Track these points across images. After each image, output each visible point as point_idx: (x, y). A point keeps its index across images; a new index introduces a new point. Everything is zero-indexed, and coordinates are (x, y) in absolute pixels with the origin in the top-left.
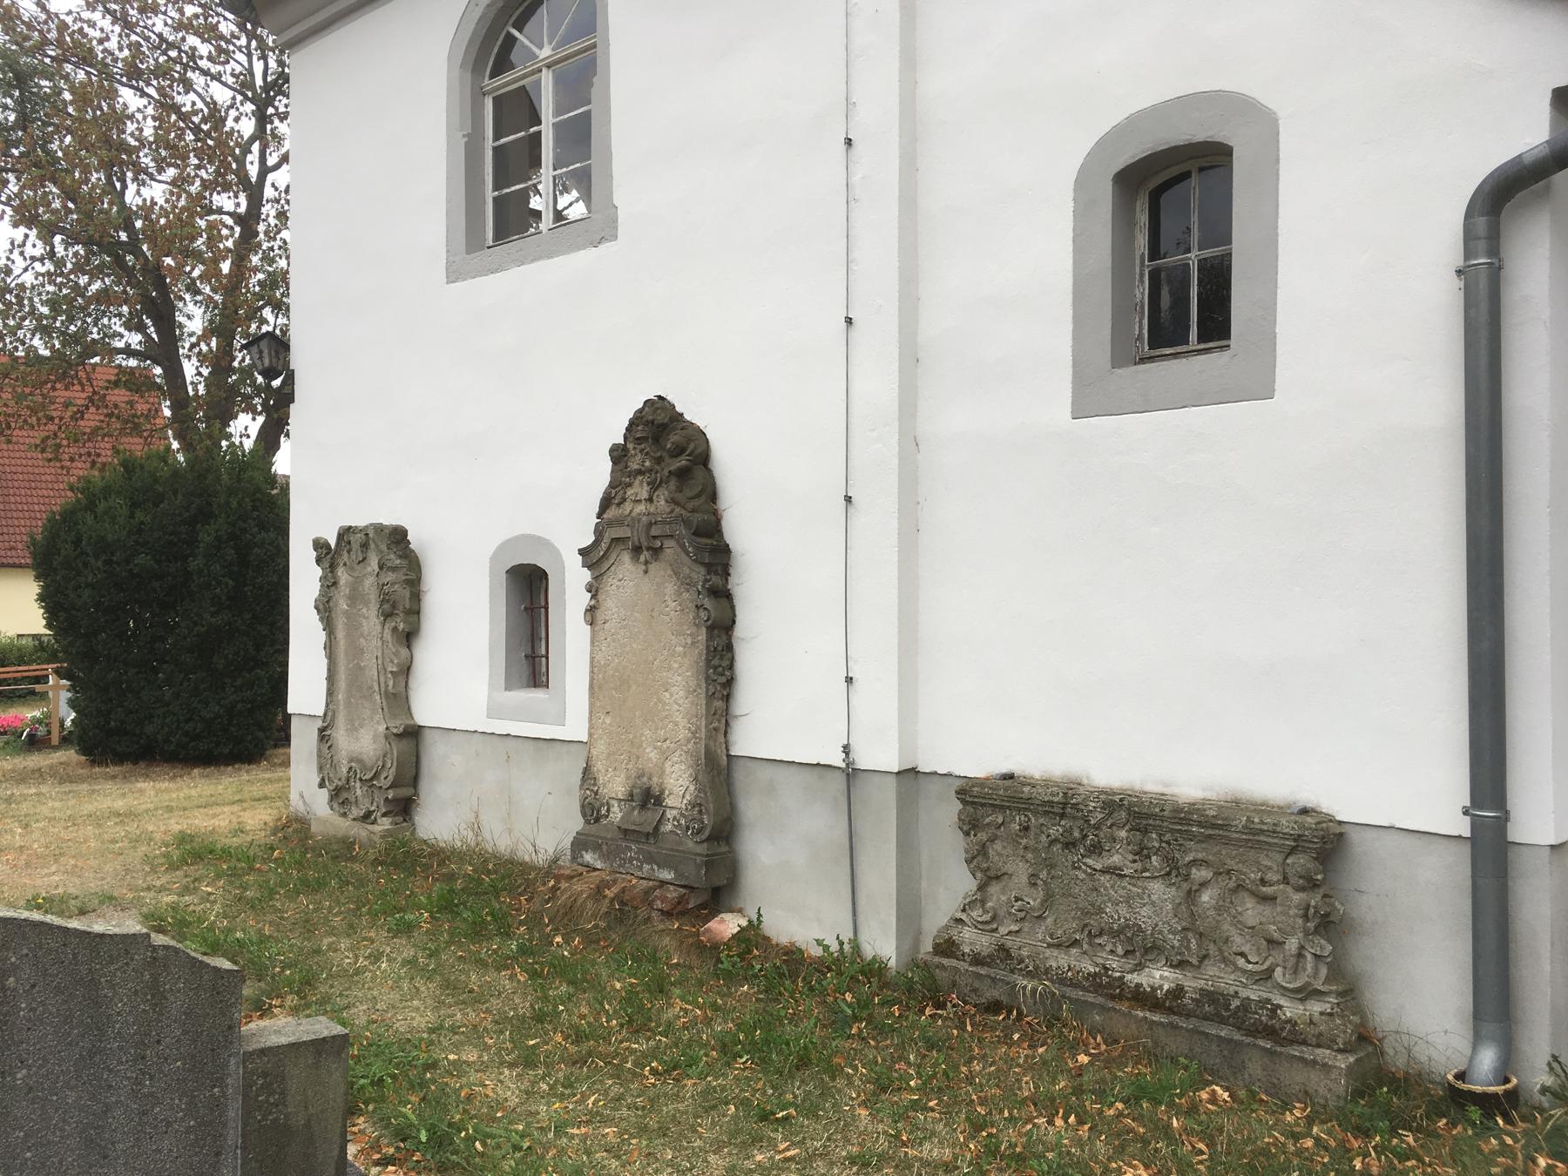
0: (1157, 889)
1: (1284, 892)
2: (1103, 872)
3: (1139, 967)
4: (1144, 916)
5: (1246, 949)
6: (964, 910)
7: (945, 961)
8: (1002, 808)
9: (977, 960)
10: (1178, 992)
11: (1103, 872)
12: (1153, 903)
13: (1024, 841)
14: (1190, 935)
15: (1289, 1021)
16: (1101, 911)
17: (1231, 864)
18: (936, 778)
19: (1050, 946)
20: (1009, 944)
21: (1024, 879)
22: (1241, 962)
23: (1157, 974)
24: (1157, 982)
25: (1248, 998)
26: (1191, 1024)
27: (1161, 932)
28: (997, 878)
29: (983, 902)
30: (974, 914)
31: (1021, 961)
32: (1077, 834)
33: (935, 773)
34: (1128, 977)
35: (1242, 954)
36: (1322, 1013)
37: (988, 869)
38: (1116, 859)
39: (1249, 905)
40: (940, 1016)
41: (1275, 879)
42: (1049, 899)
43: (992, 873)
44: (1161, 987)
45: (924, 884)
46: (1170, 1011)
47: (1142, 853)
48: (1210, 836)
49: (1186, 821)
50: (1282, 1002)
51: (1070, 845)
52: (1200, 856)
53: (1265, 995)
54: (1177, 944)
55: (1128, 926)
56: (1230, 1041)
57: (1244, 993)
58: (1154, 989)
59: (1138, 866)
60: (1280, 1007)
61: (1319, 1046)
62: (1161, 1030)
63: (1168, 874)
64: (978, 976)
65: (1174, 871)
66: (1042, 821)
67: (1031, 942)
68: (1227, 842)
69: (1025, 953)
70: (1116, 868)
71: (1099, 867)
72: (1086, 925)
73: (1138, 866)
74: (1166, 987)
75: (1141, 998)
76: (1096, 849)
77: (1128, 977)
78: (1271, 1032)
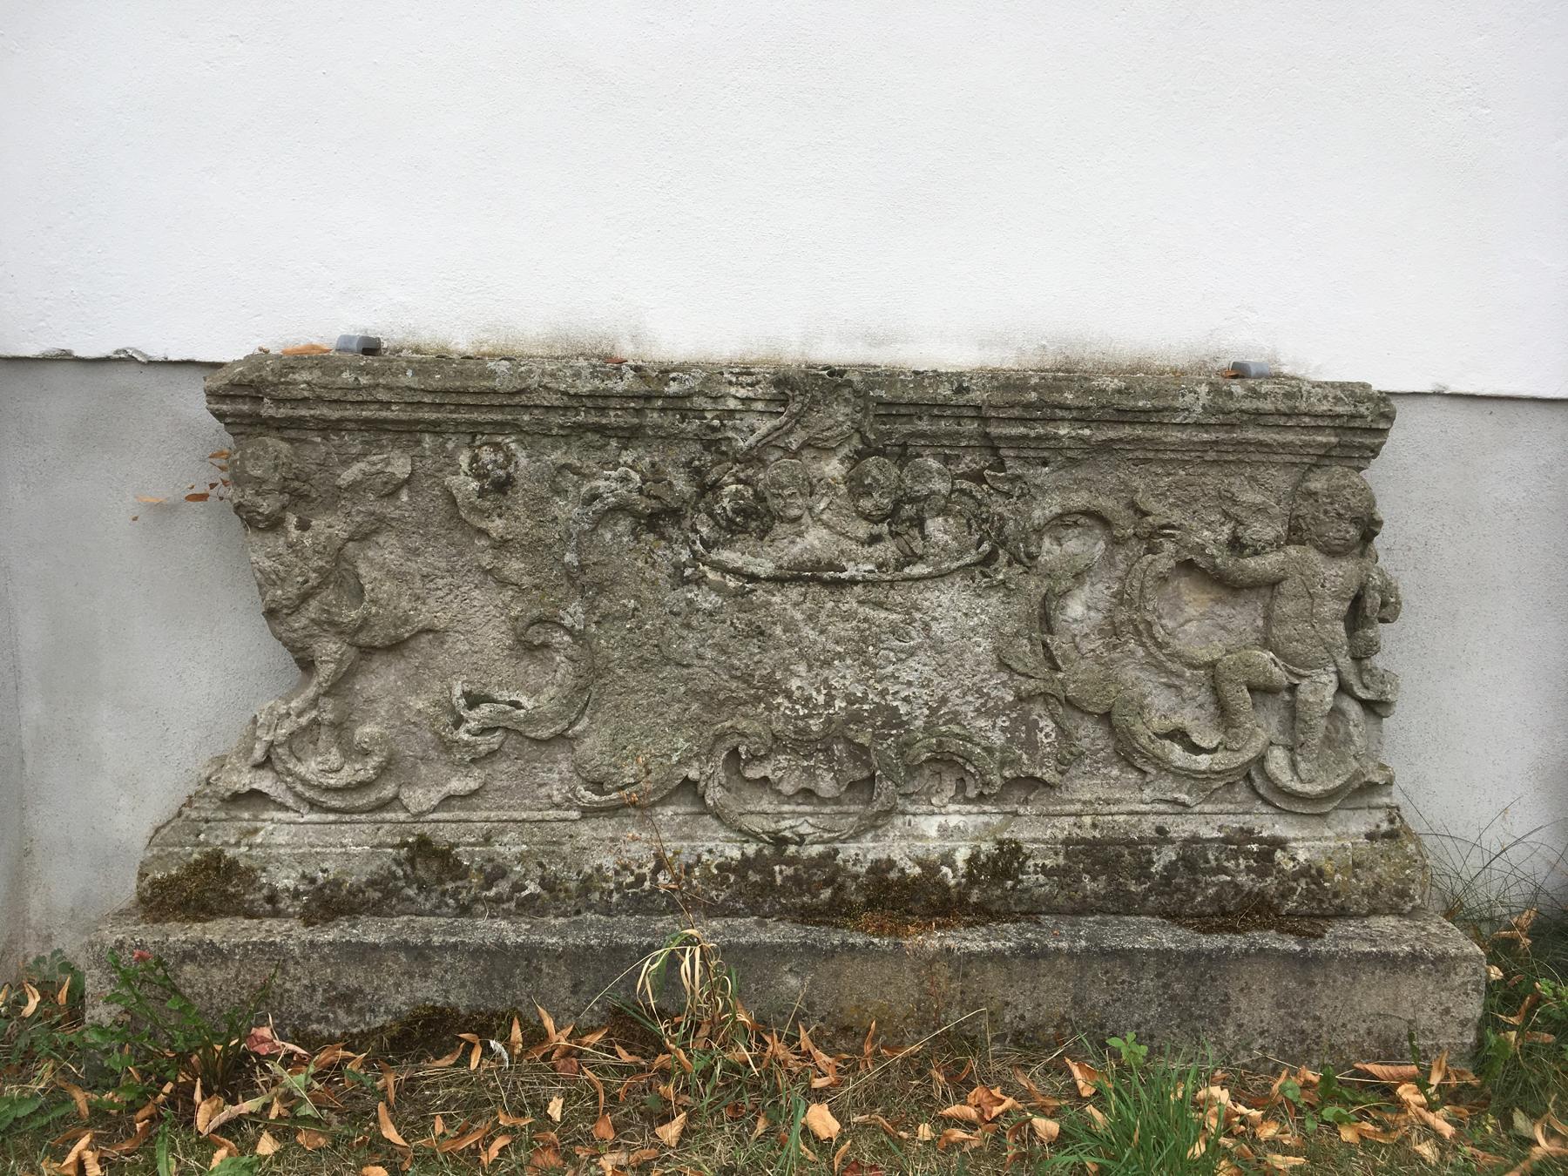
0: (951, 607)
1: (1304, 561)
2: (778, 580)
3: (874, 824)
4: (911, 683)
5: (1186, 718)
6: (266, 763)
7: (217, 931)
8: (406, 432)
9: (328, 903)
10: (1004, 863)
11: (778, 580)
12: (937, 646)
13: (496, 526)
14: (1037, 709)
15: (1304, 872)
16: (772, 687)
17: (1161, 511)
18: (60, 376)
19: (588, 812)
20: (445, 835)
21: (494, 637)
22: (1177, 754)
23: (930, 826)
24: (934, 847)
25: (1195, 839)
26: (1061, 937)
27: (955, 717)
28: (396, 647)
29: (341, 728)
30: (310, 768)
31: (497, 873)
32: (682, 485)
33: (65, 359)
34: (849, 850)
35: (1179, 735)
36: (1370, 837)
37: (365, 624)
38: (814, 541)
39: (1191, 611)
40: (258, 1119)
41: (1269, 533)
42: (587, 690)
43: (378, 636)
44: (947, 859)
45: (33, 709)
46: (984, 914)
47: (901, 517)
48: (1107, 447)
49: (1048, 410)
50: (1288, 833)
51: (658, 519)
52: (1079, 500)
53: (1234, 822)
54: (998, 739)
55: (856, 718)
56: (1193, 957)
57: (1182, 828)
58: (929, 868)
59: (888, 550)
60: (1280, 843)
61: (1374, 912)
62: (992, 973)
63: (988, 560)
64: (361, 953)
65: (997, 553)
66: (557, 457)
67: (517, 819)
68: (1150, 455)
69: (509, 847)
70: (817, 565)
71: (764, 567)
72: (720, 737)
73: (888, 550)
74: (962, 855)
75: (903, 898)
76: (756, 519)
77: (849, 850)
78: (1258, 911)
